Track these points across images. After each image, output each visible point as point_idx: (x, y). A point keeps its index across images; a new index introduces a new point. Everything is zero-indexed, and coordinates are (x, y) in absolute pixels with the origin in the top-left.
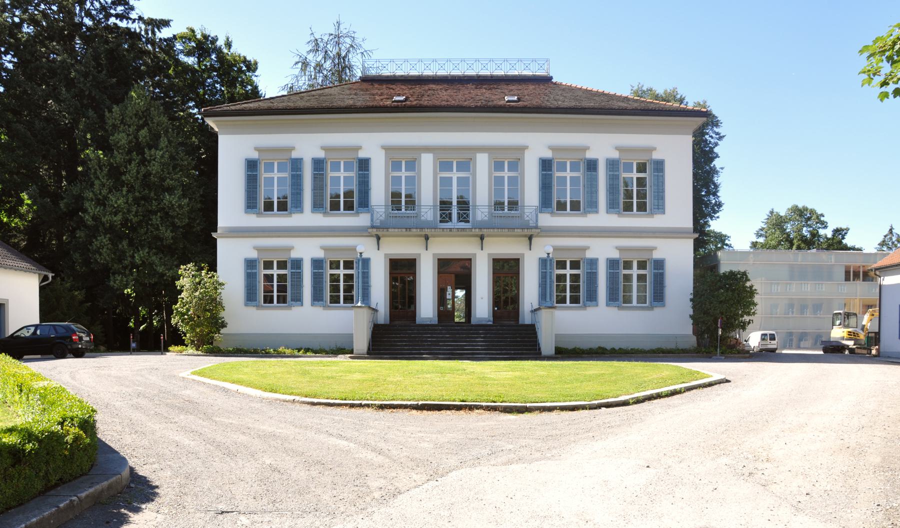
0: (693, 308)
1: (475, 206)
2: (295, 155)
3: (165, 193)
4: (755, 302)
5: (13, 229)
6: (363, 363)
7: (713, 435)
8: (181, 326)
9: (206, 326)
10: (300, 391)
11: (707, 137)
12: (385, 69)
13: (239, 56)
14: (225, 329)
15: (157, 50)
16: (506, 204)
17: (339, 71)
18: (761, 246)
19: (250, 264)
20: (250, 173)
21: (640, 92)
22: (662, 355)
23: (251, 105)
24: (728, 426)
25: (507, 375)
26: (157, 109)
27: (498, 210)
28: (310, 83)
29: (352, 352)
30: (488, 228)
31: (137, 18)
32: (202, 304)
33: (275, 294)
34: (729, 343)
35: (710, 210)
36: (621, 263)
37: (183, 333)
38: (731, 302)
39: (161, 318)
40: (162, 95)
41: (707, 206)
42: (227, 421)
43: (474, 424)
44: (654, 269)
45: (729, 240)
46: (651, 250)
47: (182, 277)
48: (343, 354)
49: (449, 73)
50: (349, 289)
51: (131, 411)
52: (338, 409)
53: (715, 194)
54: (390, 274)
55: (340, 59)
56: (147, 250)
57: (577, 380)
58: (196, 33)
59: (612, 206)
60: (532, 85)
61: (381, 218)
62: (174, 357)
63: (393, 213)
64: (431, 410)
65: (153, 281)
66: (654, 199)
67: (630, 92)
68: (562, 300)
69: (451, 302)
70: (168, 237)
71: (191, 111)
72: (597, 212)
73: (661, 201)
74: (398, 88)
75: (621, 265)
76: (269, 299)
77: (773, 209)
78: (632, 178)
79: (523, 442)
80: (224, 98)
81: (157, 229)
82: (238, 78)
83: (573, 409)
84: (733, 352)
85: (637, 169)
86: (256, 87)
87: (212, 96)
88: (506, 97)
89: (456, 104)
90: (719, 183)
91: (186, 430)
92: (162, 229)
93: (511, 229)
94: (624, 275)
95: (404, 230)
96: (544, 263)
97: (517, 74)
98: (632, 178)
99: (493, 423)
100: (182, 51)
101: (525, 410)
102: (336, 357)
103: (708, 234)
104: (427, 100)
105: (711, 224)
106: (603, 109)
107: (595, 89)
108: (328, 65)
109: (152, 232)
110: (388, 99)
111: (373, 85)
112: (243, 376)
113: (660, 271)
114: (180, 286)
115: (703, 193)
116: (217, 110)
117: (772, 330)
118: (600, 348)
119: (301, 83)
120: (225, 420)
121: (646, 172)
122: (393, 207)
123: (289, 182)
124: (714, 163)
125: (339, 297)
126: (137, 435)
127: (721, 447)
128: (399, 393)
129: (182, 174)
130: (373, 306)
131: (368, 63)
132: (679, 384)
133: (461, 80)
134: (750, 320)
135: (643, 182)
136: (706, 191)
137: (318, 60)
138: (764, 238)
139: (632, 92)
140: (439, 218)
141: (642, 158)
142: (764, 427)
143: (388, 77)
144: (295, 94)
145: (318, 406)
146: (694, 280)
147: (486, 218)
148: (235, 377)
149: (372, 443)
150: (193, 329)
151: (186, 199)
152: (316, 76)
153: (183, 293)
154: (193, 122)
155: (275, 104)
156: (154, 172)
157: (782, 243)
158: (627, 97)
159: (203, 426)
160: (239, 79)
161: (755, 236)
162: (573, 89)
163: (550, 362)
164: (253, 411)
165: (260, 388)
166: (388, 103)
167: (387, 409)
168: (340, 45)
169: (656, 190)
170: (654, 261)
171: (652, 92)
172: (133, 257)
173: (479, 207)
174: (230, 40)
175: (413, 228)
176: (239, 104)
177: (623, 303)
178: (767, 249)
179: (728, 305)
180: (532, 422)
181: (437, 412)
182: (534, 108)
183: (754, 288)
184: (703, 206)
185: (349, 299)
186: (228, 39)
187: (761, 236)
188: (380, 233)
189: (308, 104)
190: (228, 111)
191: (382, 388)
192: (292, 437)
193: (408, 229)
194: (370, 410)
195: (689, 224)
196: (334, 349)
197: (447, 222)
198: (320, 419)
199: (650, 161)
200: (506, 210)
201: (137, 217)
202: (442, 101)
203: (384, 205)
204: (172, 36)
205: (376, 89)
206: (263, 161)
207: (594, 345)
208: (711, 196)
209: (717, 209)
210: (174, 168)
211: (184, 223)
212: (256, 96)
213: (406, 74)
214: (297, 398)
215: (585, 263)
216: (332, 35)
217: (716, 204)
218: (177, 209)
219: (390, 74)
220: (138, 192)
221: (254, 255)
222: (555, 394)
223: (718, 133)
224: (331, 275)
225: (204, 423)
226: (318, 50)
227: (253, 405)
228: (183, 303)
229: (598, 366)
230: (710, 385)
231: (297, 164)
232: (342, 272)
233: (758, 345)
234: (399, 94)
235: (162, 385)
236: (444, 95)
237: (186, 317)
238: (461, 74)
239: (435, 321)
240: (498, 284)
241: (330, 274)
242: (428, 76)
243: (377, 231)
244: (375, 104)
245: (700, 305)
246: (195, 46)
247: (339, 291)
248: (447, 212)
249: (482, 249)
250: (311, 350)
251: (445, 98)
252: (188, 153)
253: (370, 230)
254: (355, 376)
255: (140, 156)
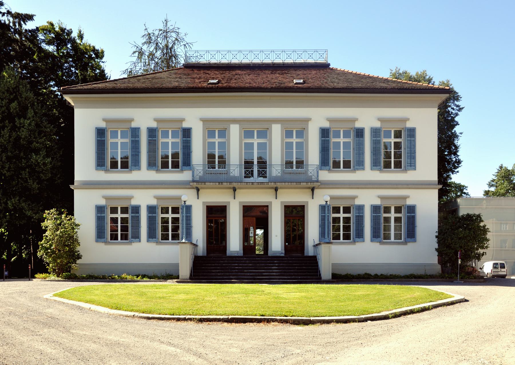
0: (438, 243)
1: (271, 165)
2: (134, 125)
3: (32, 154)
4: (488, 238)
6: (187, 286)
7: (456, 343)
8: (45, 258)
9: (65, 257)
10: (139, 308)
11: (449, 109)
12: (202, 58)
13: (90, 46)
14: (80, 260)
15: (24, 39)
16: (294, 163)
17: (167, 59)
18: (493, 194)
19: (100, 209)
20: (100, 139)
21: (397, 75)
22: (414, 279)
23: (100, 85)
24: (467, 337)
25: (295, 295)
26: (25, 87)
27: (288, 168)
28: (145, 68)
29: (178, 277)
30: (281, 182)
31: (6, 12)
32: (62, 241)
33: (119, 233)
34: (467, 270)
35: (451, 166)
36: (382, 208)
37: (47, 263)
38: (469, 238)
39: (29, 251)
40: (29, 75)
41: (449, 163)
42: (81, 333)
43: (271, 334)
44: (408, 213)
45: (467, 190)
46: (405, 198)
47: (46, 219)
48: (171, 279)
49: (251, 62)
50: (175, 229)
51: (3, 327)
52: (168, 322)
53: (455, 154)
54: (207, 217)
55: (168, 49)
56: (18, 198)
57: (348, 299)
58: (55, 27)
59: (375, 164)
60: (315, 70)
61: (200, 174)
62: (39, 282)
63: (209, 171)
64: (238, 323)
65: (23, 222)
66: (407, 159)
67: (389, 74)
68: (337, 237)
69: (253, 238)
70: (35, 188)
71: (52, 89)
72: (363, 169)
73: (413, 160)
74: (212, 73)
75: (382, 210)
76: (114, 236)
77: (502, 165)
78: (391, 142)
79: (308, 348)
80: (78, 79)
81: (26, 181)
82: (89, 63)
83: (346, 321)
84: (470, 277)
85: (394, 135)
86: (103, 71)
87: (69, 77)
88: (294, 80)
89: (256, 86)
90: (458, 145)
91: (49, 341)
92: (30, 182)
93: (298, 182)
95: (217, 184)
96: (323, 208)
97: (303, 62)
98: (391, 142)
99: (285, 333)
100: (44, 41)
101: (309, 322)
102: (166, 281)
103: (449, 185)
104: (235, 83)
105: (452, 177)
106: (368, 89)
107: (363, 73)
108: (158, 54)
109: (22, 184)
110: (205, 81)
111: (193, 71)
112: (94, 297)
113: (412, 214)
114: (44, 227)
115: (446, 153)
116: (73, 88)
117: (502, 260)
118: (366, 274)
119: (138, 68)
120: (80, 332)
121: (401, 138)
122: (209, 166)
123: (129, 146)
124: (455, 129)
125: (168, 235)
126: (8, 346)
127: (462, 354)
128: (214, 309)
129: (46, 139)
130: (194, 242)
131: (190, 53)
132: (427, 302)
133: (260, 67)
134: (484, 252)
135: (399, 146)
136: (448, 152)
137: (151, 50)
138: (495, 188)
139: (391, 74)
140: (243, 175)
141: (398, 127)
142: (497, 339)
143: (204, 64)
144: (134, 77)
145: (152, 320)
146: (439, 221)
147: (279, 175)
148: (88, 297)
149: (194, 348)
150: (55, 260)
151: (49, 158)
152: (150, 63)
153: (47, 232)
154: (54, 98)
155: (118, 85)
156: (23, 136)
157: (510, 191)
158: (387, 79)
159: (63, 338)
160: (90, 65)
161: (487, 186)
162: (345, 74)
163: (328, 285)
164: (102, 324)
165: (108, 306)
166: (205, 85)
167: (205, 322)
168: (168, 39)
169: (409, 152)
170: (407, 206)
171: (406, 75)
172: (6, 203)
173: (274, 166)
174: (82, 33)
175: (224, 182)
176: (90, 84)
177: (384, 240)
178: (497, 196)
179: (466, 241)
180: (315, 332)
181: (243, 324)
182: (315, 88)
183: (486, 228)
184: (446, 163)
185: (175, 237)
186: (80, 32)
187: (492, 186)
188: (199, 186)
189: (144, 85)
190: (81, 89)
191: (201, 306)
192: (132, 345)
193: (221, 183)
194: (192, 322)
195: (435, 177)
196: (165, 275)
197: (250, 177)
198: (154, 330)
199: (404, 129)
200: (294, 168)
201: (10, 172)
202: (246, 83)
203: (202, 164)
204: (35, 28)
205: (196, 74)
206: (110, 130)
207: (362, 272)
208: (452, 155)
209: (457, 166)
210: (40, 133)
211: (48, 177)
212: (103, 78)
213: (218, 62)
214: (137, 314)
215: (355, 208)
216: (161, 30)
217: (456, 162)
218: (42, 166)
219: (206, 62)
220: (10, 152)
221: (103, 202)
222: (332, 310)
223: (458, 105)
224: (162, 218)
225: (64, 335)
226: (151, 43)
227: (102, 320)
228: (47, 240)
229: (365, 288)
230: (452, 303)
232: (170, 216)
233: (490, 272)
234: (213, 78)
235: (30, 305)
236: (247, 79)
237: (49, 251)
238: (260, 62)
239: (241, 254)
240: (288, 225)
241: (161, 217)
242: (235, 64)
243: (197, 184)
244: (195, 85)
245: (443, 241)
246: (54, 36)
247: (168, 231)
248: (250, 170)
249: (276, 199)
250: (147, 276)
251: (248, 81)
252: (50, 122)
253: (191, 184)
254: (180, 296)
255: (12, 124)
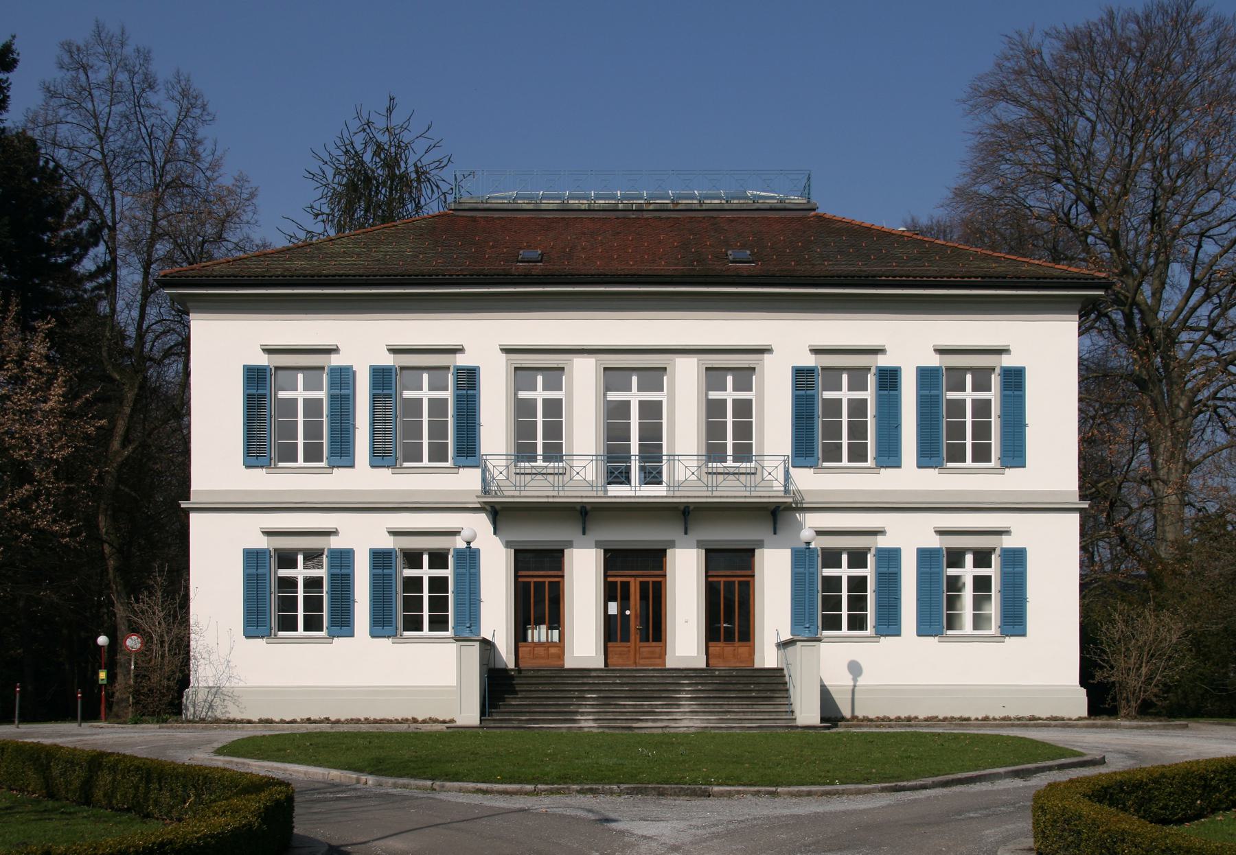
19: (253, 558)
94: (949, 578)
231: (343, 378)
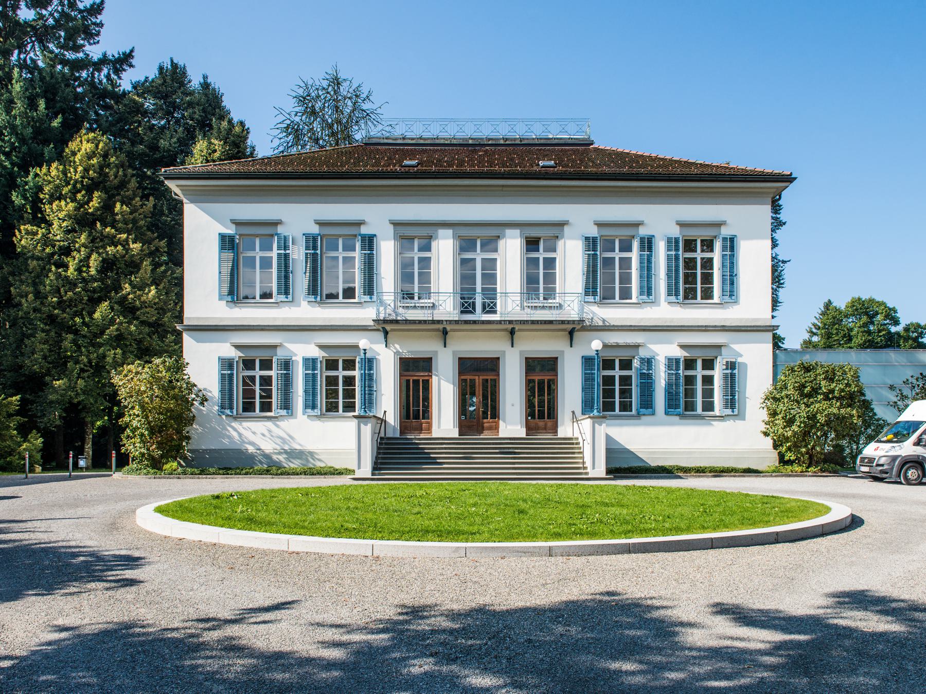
5: (73, 321)
19: (227, 364)
68: (248, 407)
173: (509, 294)
249: (512, 346)
